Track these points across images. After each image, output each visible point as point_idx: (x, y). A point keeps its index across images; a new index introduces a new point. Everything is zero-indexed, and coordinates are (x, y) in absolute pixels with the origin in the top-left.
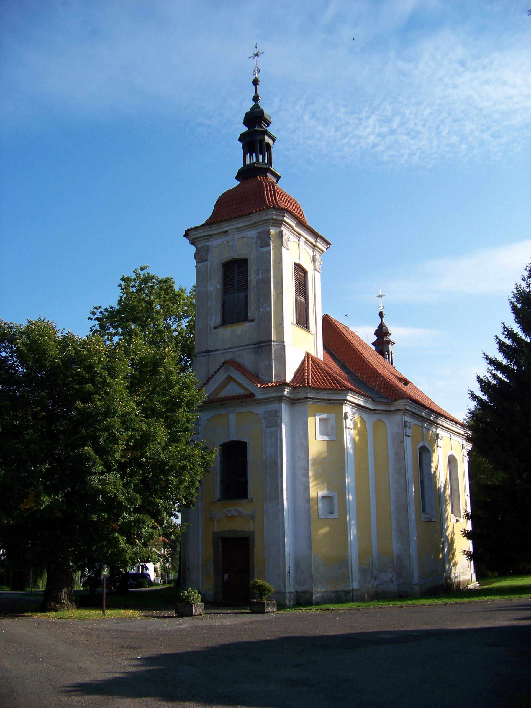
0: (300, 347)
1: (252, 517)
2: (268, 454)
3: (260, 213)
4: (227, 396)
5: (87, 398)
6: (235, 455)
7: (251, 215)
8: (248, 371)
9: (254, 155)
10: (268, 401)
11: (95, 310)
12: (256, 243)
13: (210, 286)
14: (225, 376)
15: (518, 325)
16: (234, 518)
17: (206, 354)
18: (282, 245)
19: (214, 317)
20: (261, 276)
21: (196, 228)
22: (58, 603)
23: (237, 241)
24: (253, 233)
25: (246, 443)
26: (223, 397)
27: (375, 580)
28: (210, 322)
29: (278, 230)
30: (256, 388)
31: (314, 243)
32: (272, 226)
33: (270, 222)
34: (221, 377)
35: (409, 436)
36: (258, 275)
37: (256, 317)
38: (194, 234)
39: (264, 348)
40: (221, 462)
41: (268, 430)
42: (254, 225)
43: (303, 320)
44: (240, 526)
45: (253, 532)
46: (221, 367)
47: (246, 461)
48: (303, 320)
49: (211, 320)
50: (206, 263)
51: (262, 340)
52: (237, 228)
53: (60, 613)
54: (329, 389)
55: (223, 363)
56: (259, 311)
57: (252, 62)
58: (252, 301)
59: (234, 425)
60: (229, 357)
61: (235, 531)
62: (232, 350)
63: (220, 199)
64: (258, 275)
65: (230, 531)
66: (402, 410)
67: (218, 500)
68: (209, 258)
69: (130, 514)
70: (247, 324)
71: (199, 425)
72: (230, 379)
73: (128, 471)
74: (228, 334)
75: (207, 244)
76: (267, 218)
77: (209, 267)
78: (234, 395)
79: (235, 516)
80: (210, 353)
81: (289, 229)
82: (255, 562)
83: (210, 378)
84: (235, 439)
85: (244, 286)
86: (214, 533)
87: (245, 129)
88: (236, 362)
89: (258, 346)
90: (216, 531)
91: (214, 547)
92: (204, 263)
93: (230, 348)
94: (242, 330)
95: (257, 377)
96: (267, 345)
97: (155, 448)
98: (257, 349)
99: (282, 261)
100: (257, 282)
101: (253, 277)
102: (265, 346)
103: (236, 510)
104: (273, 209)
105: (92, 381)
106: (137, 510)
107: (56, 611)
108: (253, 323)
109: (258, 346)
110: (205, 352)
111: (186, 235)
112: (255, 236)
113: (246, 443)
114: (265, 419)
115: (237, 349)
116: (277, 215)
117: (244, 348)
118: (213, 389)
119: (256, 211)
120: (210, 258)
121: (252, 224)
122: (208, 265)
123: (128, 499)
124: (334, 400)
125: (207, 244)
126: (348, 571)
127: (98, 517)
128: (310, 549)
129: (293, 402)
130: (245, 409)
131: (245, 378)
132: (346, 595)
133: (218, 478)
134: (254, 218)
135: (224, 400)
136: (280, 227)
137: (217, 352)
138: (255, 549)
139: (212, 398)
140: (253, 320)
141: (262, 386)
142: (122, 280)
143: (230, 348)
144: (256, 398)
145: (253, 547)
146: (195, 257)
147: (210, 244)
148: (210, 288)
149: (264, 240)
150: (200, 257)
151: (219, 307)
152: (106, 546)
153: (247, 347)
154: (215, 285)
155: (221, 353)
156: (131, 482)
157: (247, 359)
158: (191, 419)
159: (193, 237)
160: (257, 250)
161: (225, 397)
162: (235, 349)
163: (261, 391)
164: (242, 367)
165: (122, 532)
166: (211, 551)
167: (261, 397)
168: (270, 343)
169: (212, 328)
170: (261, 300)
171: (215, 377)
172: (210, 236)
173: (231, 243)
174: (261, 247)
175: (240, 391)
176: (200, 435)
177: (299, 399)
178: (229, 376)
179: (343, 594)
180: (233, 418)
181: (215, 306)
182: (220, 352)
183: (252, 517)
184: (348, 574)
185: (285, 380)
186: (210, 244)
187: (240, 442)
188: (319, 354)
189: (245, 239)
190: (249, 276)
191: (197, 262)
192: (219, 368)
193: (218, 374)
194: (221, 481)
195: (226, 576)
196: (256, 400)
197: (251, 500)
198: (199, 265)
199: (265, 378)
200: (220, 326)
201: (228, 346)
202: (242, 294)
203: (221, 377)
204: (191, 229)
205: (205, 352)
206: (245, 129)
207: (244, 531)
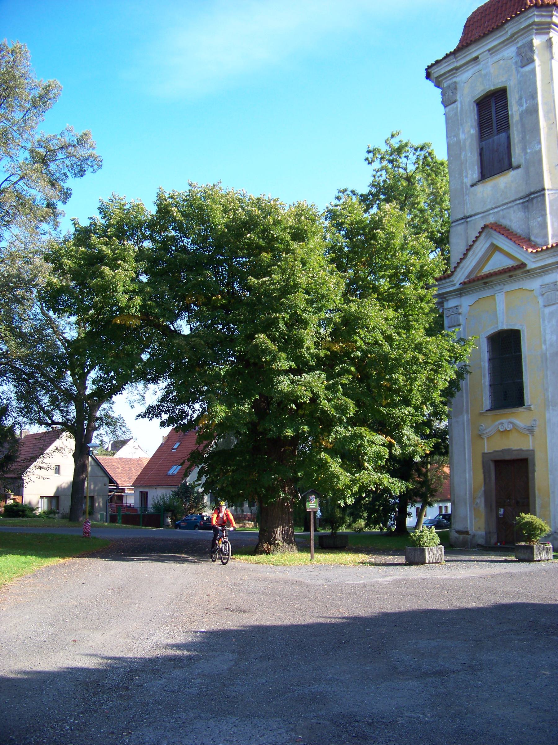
1: (531, 430)
2: (548, 343)
3: (517, 19)
4: (492, 271)
5: (262, 271)
7: (505, 26)
8: (516, 234)
11: (341, 194)
12: (516, 62)
13: (463, 133)
14: (487, 245)
16: (509, 433)
17: (463, 221)
18: (552, 58)
19: (470, 172)
20: (525, 106)
21: (437, 62)
22: (270, 543)
23: (492, 68)
24: (510, 51)
28: (465, 180)
29: (545, 38)
30: (524, 254)
32: (536, 34)
33: (532, 29)
34: (481, 247)
36: (521, 105)
37: (523, 161)
38: (436, 72)
39: (535, 201)
40: (490, 360)
41: (547, 310)
42: (512, 39)
44: (516, 444)
45: (533, 451)
46: (480, 233)
47: (522, 382)
49: (466, 177)
51: (532, 190)
52: (489, 50)
53: (271, 557)
56: (526, 153)
58: (516, 141)
59: (503, 309)
60: (491, 219)
61: (509, 451)
62: (496, 210)
63: (469, 20)
64: (521, 105)
65: (503, 451)
68: (458, 98)
69: (346, 428)
71: (460, 314)
72: (494, 248)
73: (338, 369)
75: (454, 80)
76: (527, 23)
77: (459, 109)
79: (509, 431)
80: (468, 220)
82: (537, 492)
83: (468, 250)
84: (505, 327)
85: (504, 124)
86: (484, 454)
88: (501, 225)
89: (527, 199)
90: (486, 451)
91: (484, 473)
92: (453, 105)
93: (492, 209)
94: (506, 183)
95: (529, 240)
96: (540, 196)
97: (372, 336)
98: (526, 204)
99: (552, 79)
100: (521, 116)
101: (515, 110)
103: (510, 423)
104: (534, 8)
105: (270, 248)
106: (353, 422)
107: (267, 553)
108: (519, 171)
109: (527, 199)
110: (462, 219)
111: (428, 76)
112: (514, 54)
114: (543, 295)
115: (501, 208)
116: (542, 16)
117: (509, 205)
118: (473, 264)
119: (511, 17)
120: (460, 97)
121: (507, 39)
122: (457, 107)
123: (337, 408)
125: (454, 80)
127: (296, 430)
130: (515, 286)
131: (512, 243)
133: (486, 381)
134: (510, 29)
136: (548, 33)
137: (477, 217)
138: (536, 474)
139: (473, 276)
140: (518, 167)
141: (534, 251)
143: (492, 209)
144: (528, 268)
145: (534, 471)
147: (457, 80)
148: (462, 136)
149: (526, 57)
152: (316, 471)
153: (513, 204)
154: (469, 130)
155: (482, 217)
156: (336, 383)
157: (514, 219)
158: (425, 296)
159: (436, 75)
160: (518, 72)
161: (490, 273)
162: (499, 209)
163: (534, 258)
164: (508, 230)
165: (333, 452)
166: (481, 477)
168: (542, 193)
169: (469, 187)
170: (528, 137)
171: (474, 247)
172: (457, 69)
173: (483, 72)
174: (522, 67)
175: (508, 263)
178: (492, 245)
181: (471, 157)
182: (480, 216)
183: (531, 430)
186: (457, 80)
187: (512, 331)
189: (501, 62)
190: (509, 109)
193: (477, 243)
194: (490, 385)
195: (501, 511)
196: (528, 271)
197: (529, 408)
198: (447, 109)
199: (539, 241)
200: (479, 181)
201: (489, 207)
202: (503, 135)
203: (481, 247)
204: (432, 65)
207: (521, 450)
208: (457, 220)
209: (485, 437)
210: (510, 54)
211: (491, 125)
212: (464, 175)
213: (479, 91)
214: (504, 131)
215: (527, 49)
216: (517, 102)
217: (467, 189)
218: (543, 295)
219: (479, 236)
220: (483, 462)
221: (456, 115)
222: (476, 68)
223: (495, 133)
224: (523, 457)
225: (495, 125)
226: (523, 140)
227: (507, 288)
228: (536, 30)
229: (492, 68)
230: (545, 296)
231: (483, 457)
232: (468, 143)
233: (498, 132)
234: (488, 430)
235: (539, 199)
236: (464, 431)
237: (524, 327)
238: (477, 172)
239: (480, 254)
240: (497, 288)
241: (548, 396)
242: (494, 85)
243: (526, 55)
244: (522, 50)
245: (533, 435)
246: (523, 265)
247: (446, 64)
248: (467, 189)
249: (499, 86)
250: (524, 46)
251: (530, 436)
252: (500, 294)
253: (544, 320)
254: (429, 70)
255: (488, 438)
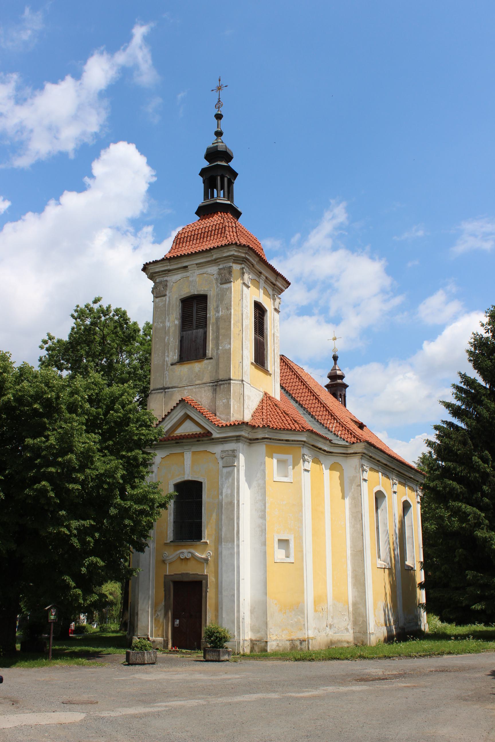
0: (252, 392)
4: (183, 434)
6: (190, 495)
9: (215, 190)
10: (225, 440)
13: (168, 321)
14: (182, 414)
15: (477, 371)
19: (171, 354)
24: (213, 270)
25: (202, 483)
26: (179, 435)
27: (330, 628)
28: (167, 359)
31: (274, 282)
33: (231, 259)
35: (308, 471)
39: (222, 387)
41: (225, 470)
42: (215, 262)
43: (260, 360)
44: (192, 569)
47: (201, 501)
48: (260, 360)
49: (168, 356)
50: (164, 298)
52: (197, 264)
54: (288, 429)
55: (180, 401)
56: (218, 349)
57: (216, 94)
62: (190, 387)
65: (182, 574)
66: (359, 453)
67: (171, 542)
70: (206, 362)
72: (187, 417)
74: (184, 370)
75: (165, 278)
76: (228, 254)
78: (191, 434)
80: (166, 390)
81: (250, 266)
84: (190, 479)
85: (203, 323)
86: (166, 576)
87: (206, 164)
90: (168, 573)
91: (165, 591)
92: (162, 298)
101: (211, 314)
102: (223, 384)
103: (190, 552)
108: (211, 361)
109: (216, 384)
110: (161, 389)
113: (202, 483)
114: (222, 458)
118: (169, 426)
120: (169, 293)
121: (212, 260)
124: (292, 441)
126: (304, 618)
128: (266, 594)
129: (251, 442)
130: (201, 448)
132: (301, 643)
135: (180, 439)
142: (76, 311)
146: (153, 292)
148: (168, 324)
150: (158, 293)
151: (177, 343)
154: (173, 320)
159: (151, 271)
160: (217, 286)
161: (181, 435)
163: (218, 430)
167: (218, 436)
168: (229, 381)
169: (169, 365)
172: (169, 271)
173: (191, 279)
174: (221, 284)
175: (196, 430)
176: (154, 474)
177: (257, 439)
178: (186, 414)
179: (298, 643)
180: (188, 456)
184: (304, 621)
185: (243, 419)
188: (277, 394)
189: (205, 275)
191: (156, 297)
192: (175, 405)
194: (174, 522)
195: (177, 622)
196: (213, 439)
202: (201, 331)
205: (161, 389)
206: (206, 164)
207: (197, 574)
208: (157, 389)
209: (167, 562)
210: (212, 272)
211: (192, 321)
212: (166, 354)
213: (185, 292)
214: (202, 328)
215: (226, 271)
216: (214, 309)
217: (167, 366)
218: (222, 458)
219: (177, 406)
220: (165, 582)
221: (164, 306)
222: (185, 274)
223: (195, 327)
224: (198, 580)
225: (195, 322)
226: (217, 339)
227: (195, 449)
228: (234, 260)
229: (198, 280)
230: (224, 459)
231: (165, 578)
232: (171, 331)
233: (197, 327)
234: (171, 557)
235: (225, 386)
236: (150, 557)
237: (206, 480)
238: (177, 355)
239: (175, 420)
240: (186, 447)
241: (222, 535)
242: (197, 291)
243: (225, 275)
244: (222, 271)
245: (207, 563)
246: (208, 434)
247: (162, 265)
248: (167, 366)
249: (202, 293)
250: (224, 269)
251: (205, 564)
252: (188, 453)
253: (222, 477)
254: (147, 266)
255: (169, 564)
